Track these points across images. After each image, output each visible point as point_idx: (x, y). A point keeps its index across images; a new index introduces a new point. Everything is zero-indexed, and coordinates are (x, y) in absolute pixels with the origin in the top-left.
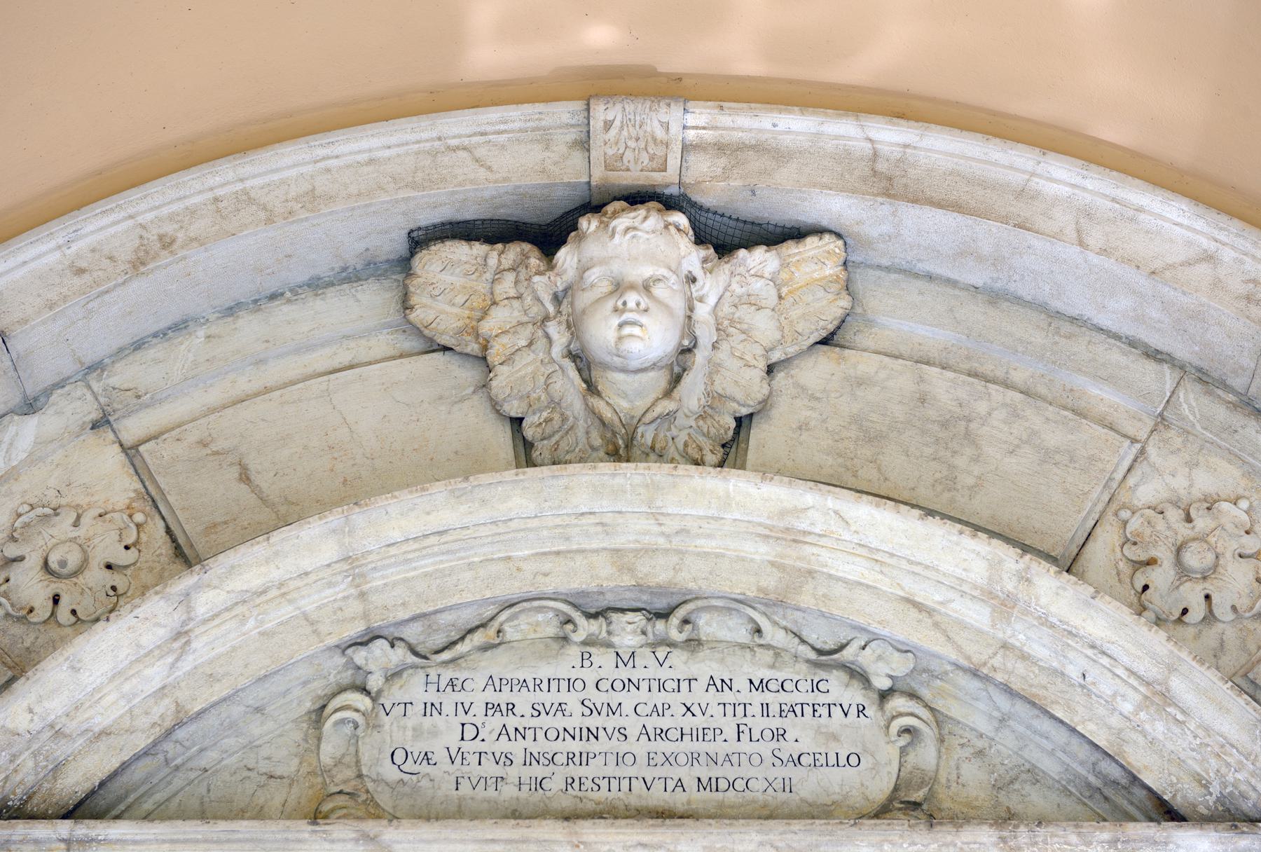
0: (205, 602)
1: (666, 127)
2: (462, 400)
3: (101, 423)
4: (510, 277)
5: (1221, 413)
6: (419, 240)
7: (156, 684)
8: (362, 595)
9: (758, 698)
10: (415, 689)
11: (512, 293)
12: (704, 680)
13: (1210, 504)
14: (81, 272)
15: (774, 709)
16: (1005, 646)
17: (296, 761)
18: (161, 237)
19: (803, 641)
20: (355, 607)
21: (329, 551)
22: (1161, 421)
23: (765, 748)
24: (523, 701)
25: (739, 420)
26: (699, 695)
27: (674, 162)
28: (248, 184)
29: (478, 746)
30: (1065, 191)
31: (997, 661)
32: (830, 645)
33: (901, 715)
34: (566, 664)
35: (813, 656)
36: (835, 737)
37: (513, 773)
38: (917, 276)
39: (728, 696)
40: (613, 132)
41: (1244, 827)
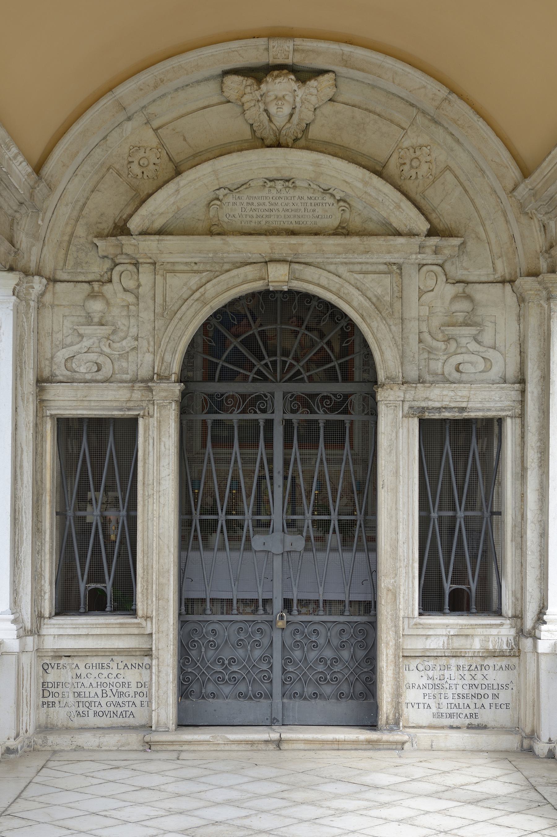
0: (182, 183)
1: (289, 47)
3: (148, 122)
4: (249, 88)
6: (226, 73)
7: (172, 202)
8: (218, 179)
9: (309, 201)
10: (230, 199)
11: (250, 92)
12: (297, 197)
13: (421, 147)
14: (141, 90)
15: (313, 204)
16: (366, 192)
17: (204, 216)
18: (160, 79)
19: (320, 188)
23: (311, 214)
24: (255, 202)
25: (307, 124)
27: (291, 57)
28: (181, 63)
29: (245, 213)
30: (391, 66)
31: (363, 196)
32: (327, 188)
33: (342, 206)
34: (265, 193)
35: (322, 191)
37: (254, 220)
39: (303, 201)
40: (275, 49)
41: (412, 237)
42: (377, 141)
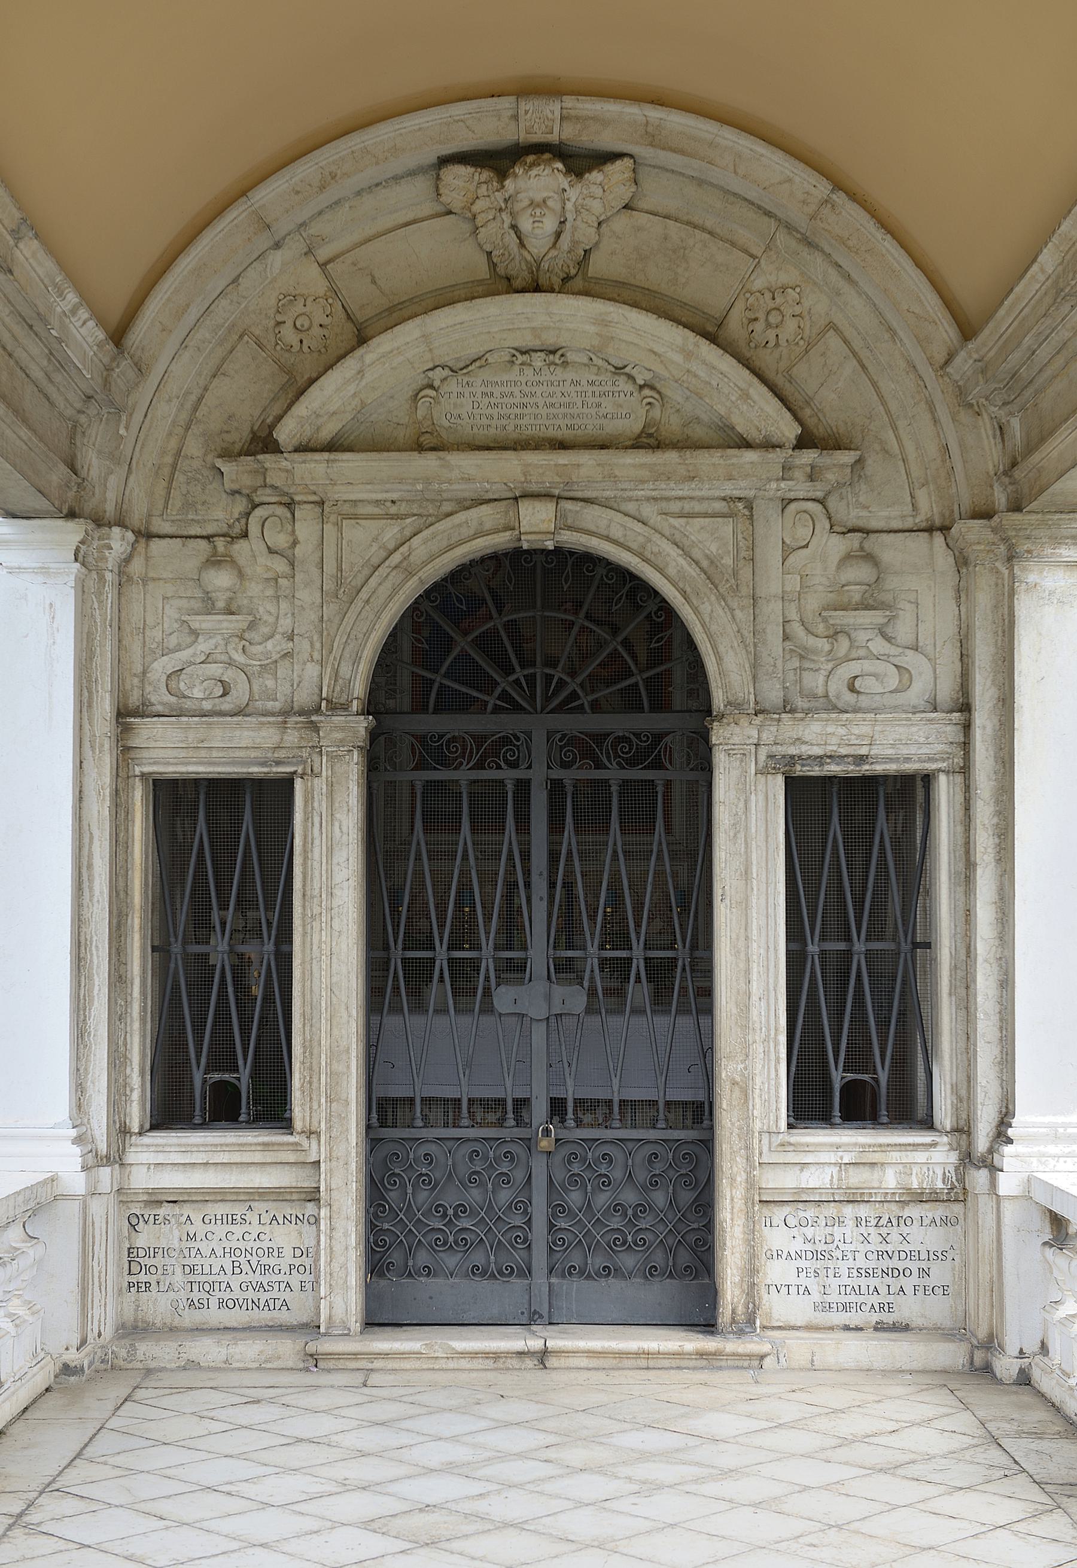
0: (369, 358)
2: (465, 240)
3: (309, 252)
4: (484, 186)
5: (793, 244)
6: (445, 161)
7: (352, 392)
9: (591, 389)
10: (452, 386)
11: (486, 194)
13: (784, 289)
14: (298, 192)
15: (597, 394)
20: (428, 356)
21: (417, 333)
22: (768, 248)
23: (593, 411)
24: (497, 391)
25: (585, 251)
26: (568, 388)
27: (556, 129)
32: (620, 365)
34: (514, 374)
35: (613, 370)
36: (621, 406)
38: (667, 170)
39: (579, 388)
40: (529, 115)
41: (770, 450)
42: (706, 281)
